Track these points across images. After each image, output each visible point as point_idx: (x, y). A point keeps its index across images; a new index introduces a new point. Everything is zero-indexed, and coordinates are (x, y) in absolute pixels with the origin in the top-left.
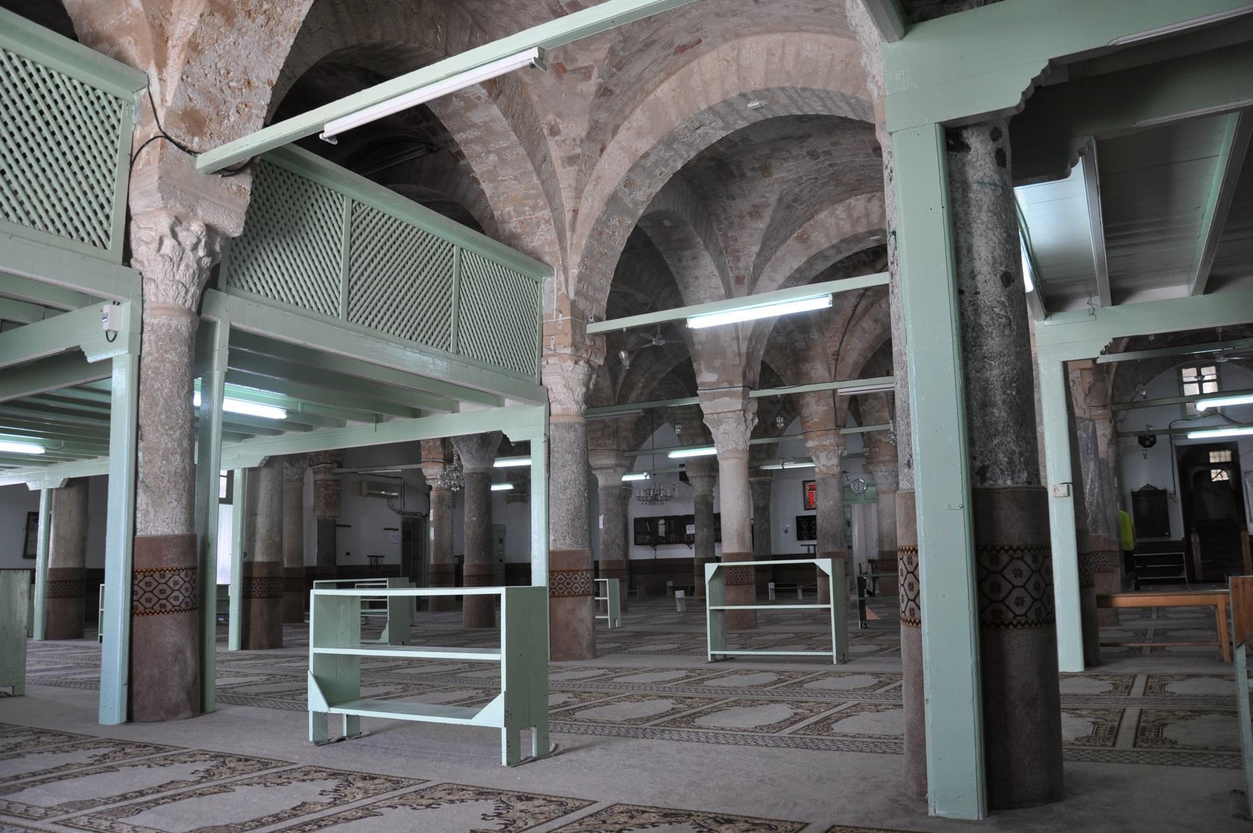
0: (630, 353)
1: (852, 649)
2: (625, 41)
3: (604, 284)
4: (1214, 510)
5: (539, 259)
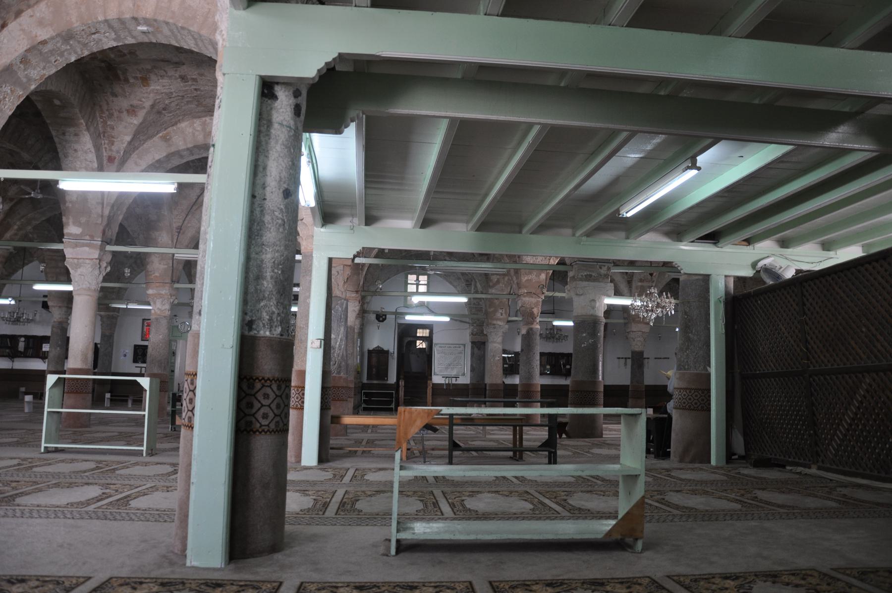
1: (159, 446)
4: (415, 366)
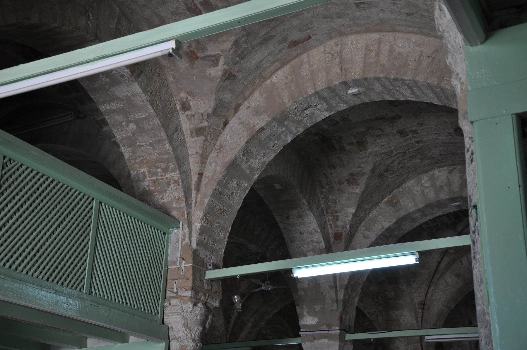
0: (242, 296)
2: (248, 35)
3: (222, 236)
5: (167, 213)
